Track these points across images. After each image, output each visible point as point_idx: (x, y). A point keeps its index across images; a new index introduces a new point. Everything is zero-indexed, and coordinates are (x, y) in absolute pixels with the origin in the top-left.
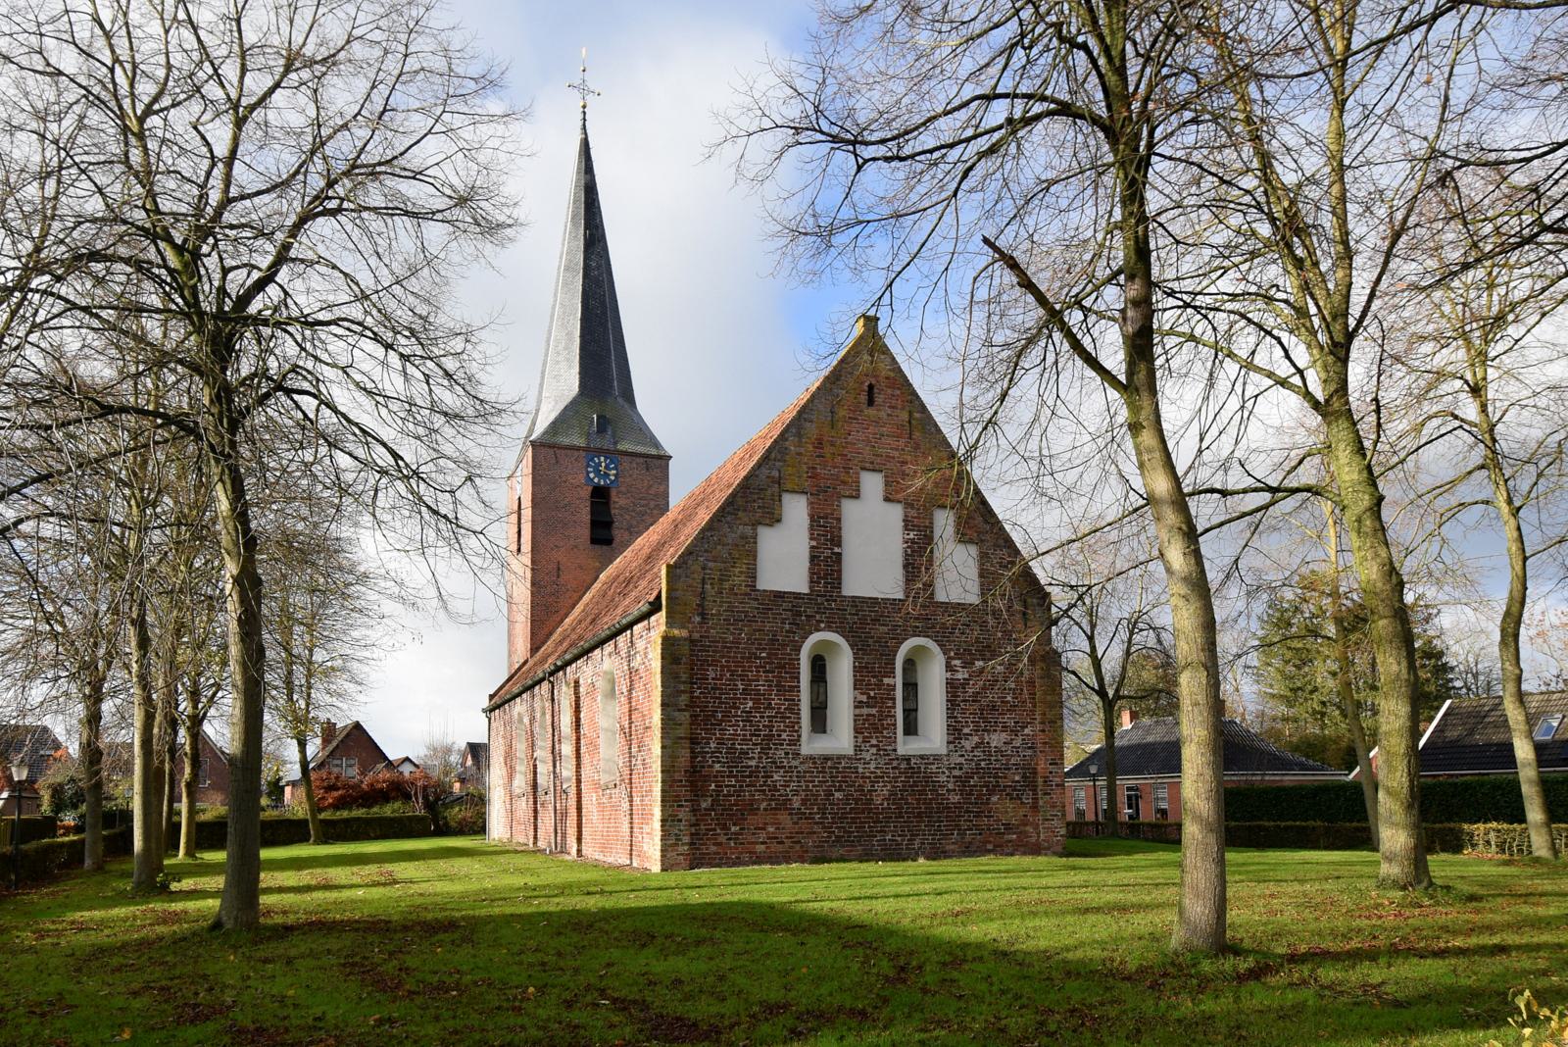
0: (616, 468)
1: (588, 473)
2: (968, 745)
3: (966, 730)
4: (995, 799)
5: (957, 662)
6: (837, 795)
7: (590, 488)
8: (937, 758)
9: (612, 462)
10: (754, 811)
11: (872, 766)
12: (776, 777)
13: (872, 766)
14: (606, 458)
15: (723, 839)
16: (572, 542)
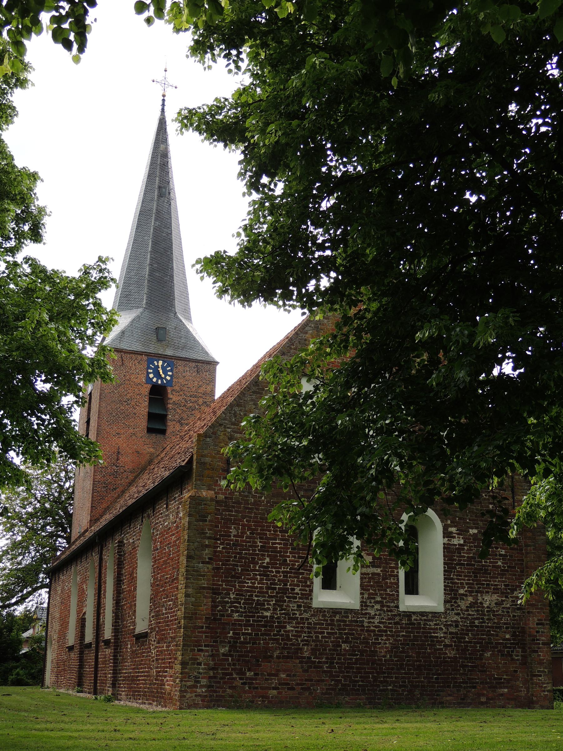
0: (171, 370)
1: (148, 373)
2: (463, 605)
3: (461, 591)
4: (488, 654)
5: (453, 530)
6: (344, 646)
7: (149, 386)
8: (435, 615)
9: (169, 365)
10: (268, 658)
11: (376, 621)
12: (289, 628)
13: (376, 621)
14: (164, 362)
15: (238, 683)
16: (131, 430)
